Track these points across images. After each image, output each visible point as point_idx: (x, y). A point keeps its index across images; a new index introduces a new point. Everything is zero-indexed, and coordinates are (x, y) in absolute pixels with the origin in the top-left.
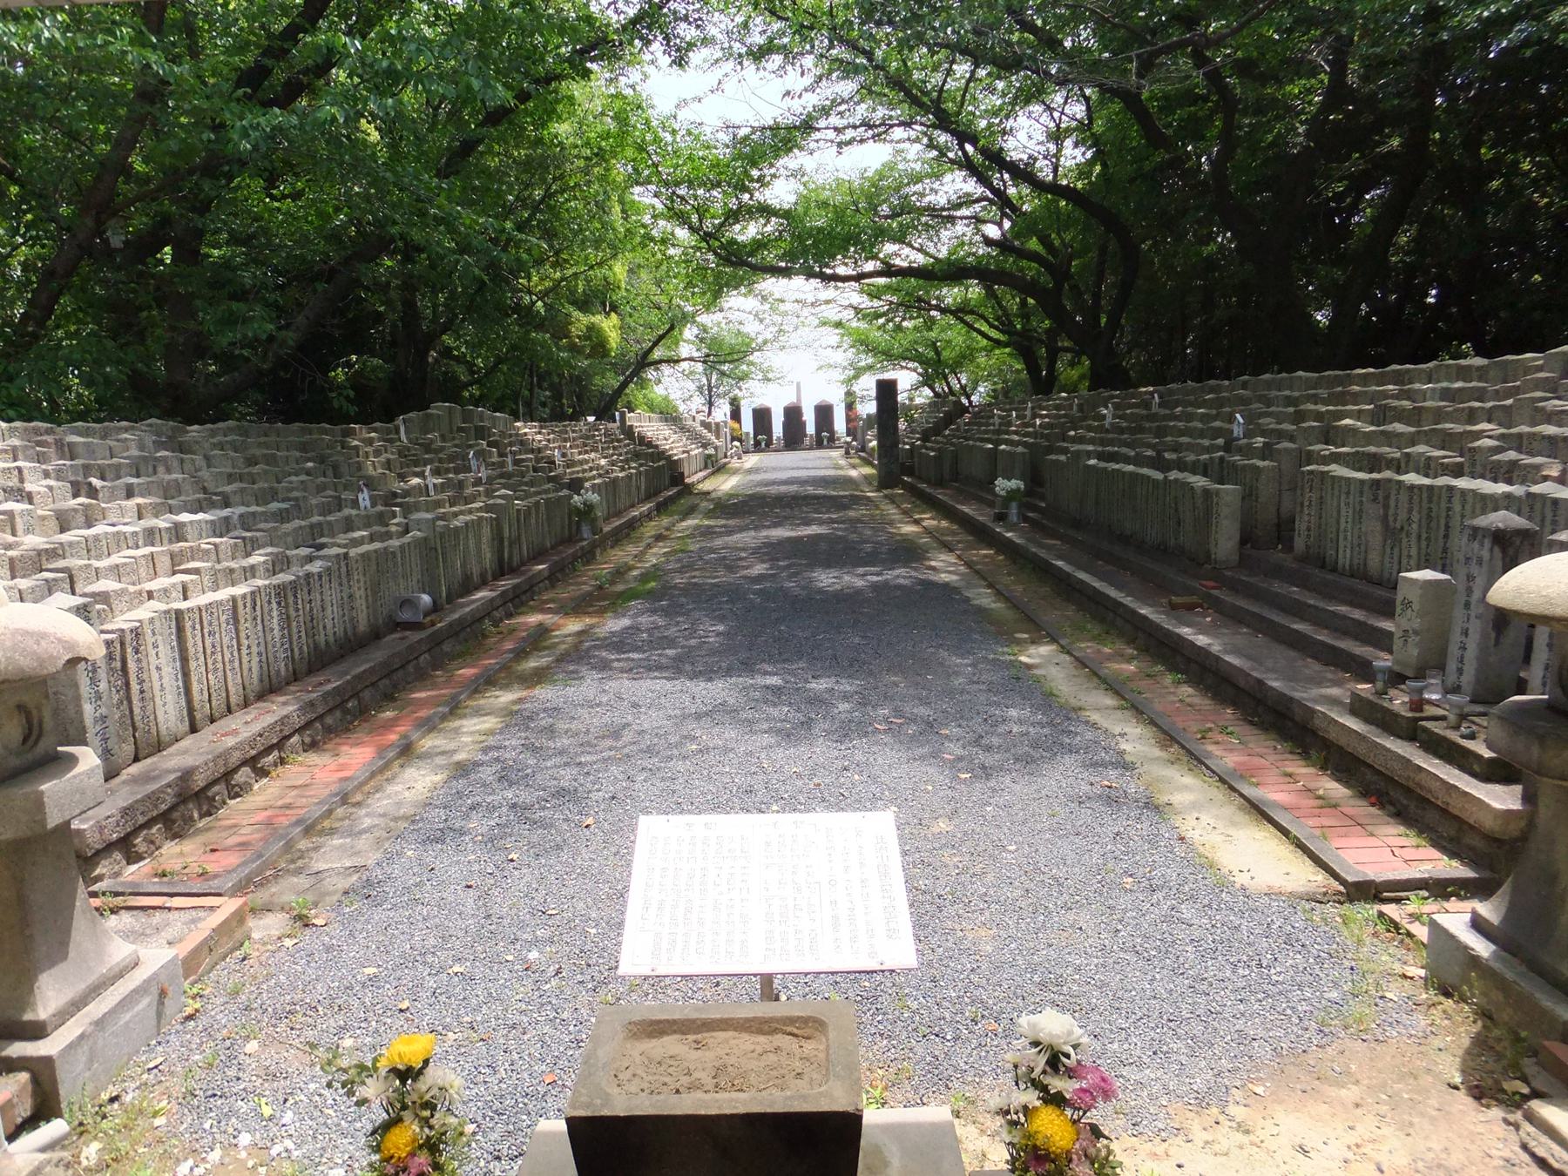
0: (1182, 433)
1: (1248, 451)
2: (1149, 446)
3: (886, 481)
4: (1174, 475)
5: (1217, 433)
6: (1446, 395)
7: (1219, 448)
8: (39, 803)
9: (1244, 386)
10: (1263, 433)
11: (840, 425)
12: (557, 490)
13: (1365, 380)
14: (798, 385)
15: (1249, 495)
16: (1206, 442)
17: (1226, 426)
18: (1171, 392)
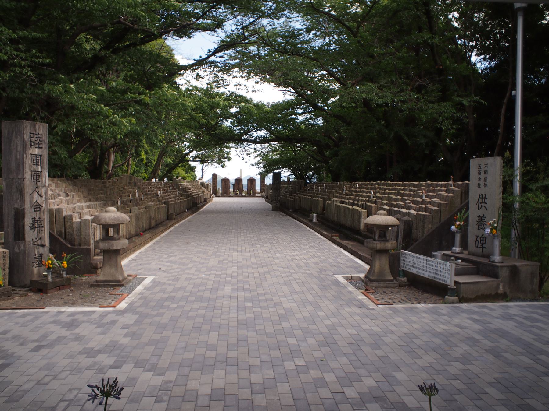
0: (361, 196)
1: (371, 202)
4: (354, 207)
6: (410, 191)
9: (378, 184)
11: (258, 188)
12: (159, 204)
13: (399, 185)
14: (241, 170)
16: (364, 199)
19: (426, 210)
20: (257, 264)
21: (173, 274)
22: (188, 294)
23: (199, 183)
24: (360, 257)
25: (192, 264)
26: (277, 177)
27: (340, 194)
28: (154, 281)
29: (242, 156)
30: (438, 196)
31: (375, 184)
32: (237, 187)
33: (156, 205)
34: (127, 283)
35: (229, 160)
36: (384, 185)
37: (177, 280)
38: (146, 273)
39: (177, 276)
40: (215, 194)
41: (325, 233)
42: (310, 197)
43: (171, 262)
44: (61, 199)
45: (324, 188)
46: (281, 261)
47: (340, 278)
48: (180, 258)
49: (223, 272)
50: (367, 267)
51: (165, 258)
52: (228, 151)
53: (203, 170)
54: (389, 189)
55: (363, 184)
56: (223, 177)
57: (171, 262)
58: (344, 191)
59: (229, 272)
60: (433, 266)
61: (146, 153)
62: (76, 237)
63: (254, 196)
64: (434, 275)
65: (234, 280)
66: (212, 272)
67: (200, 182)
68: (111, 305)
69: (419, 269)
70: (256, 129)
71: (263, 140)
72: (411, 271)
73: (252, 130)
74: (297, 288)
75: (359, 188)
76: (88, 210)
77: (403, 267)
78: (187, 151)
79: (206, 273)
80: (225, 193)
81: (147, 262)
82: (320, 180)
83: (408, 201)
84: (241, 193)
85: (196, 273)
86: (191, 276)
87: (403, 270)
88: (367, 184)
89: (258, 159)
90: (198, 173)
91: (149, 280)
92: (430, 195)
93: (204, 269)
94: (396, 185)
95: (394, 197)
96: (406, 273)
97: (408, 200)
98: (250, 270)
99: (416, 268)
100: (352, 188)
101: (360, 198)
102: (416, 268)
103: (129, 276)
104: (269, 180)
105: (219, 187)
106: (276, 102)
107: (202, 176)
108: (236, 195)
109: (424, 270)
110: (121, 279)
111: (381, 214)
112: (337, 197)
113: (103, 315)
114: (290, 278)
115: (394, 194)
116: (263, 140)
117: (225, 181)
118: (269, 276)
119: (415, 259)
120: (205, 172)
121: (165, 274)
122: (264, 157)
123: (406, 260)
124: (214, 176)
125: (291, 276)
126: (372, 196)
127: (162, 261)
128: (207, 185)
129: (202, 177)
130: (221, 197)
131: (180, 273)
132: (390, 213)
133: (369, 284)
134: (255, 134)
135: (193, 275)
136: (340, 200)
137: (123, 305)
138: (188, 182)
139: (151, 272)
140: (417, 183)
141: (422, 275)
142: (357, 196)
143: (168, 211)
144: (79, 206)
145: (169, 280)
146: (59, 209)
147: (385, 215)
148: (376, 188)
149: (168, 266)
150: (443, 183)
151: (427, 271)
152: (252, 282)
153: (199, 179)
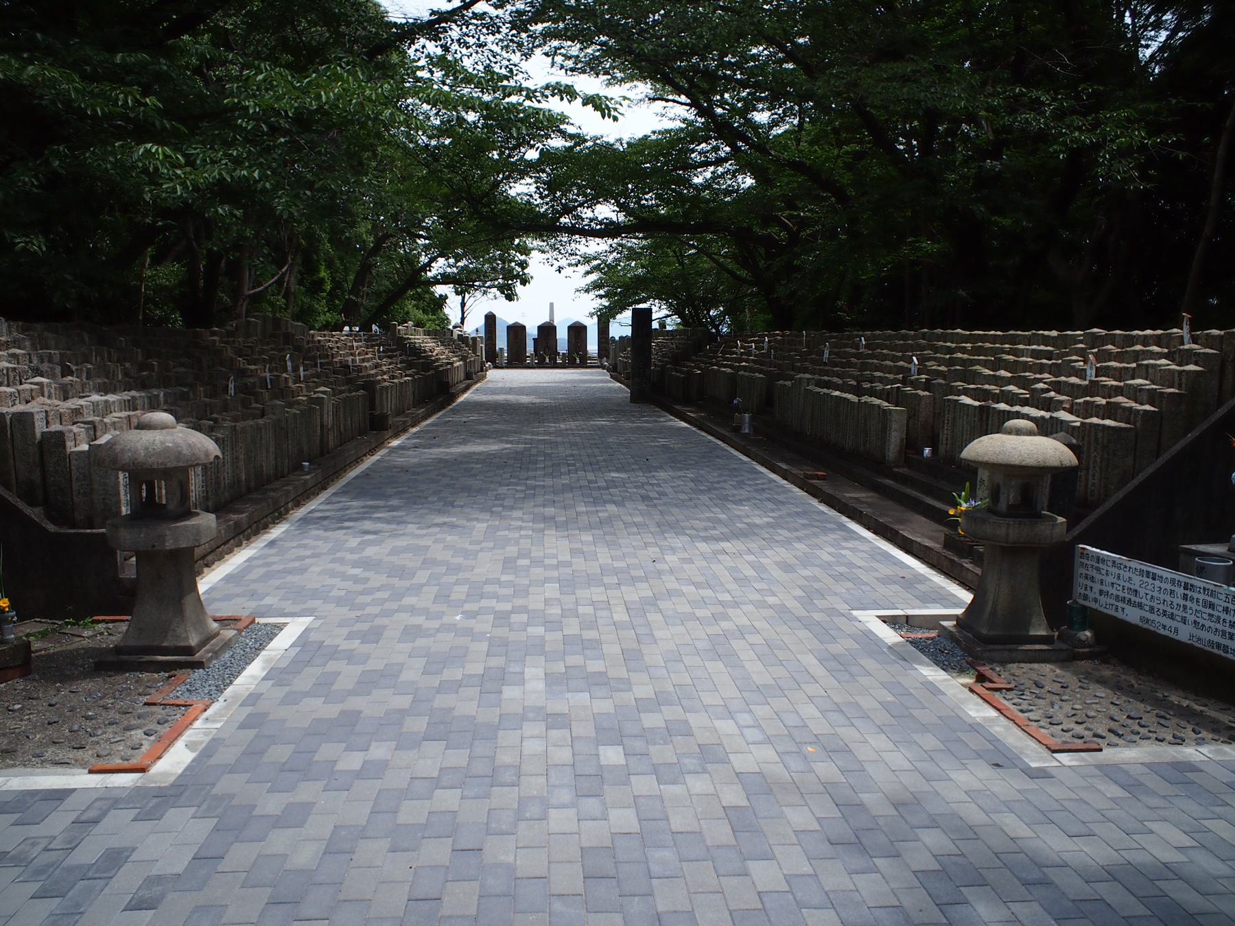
0: (877, 369)
1: (915, 384)
2: (853, 378)
3: (638, 397)
4: (865, 399)
5: (901, 370)
6: (1036, 354)
7: (898, 381)
8: (162, 537)
9: (924, 336)
10: (928, 372)
11: (592, 346)
12: (350, 392)
13: (994, 339)
14: (552, 305)
15: (912, 415)
16: (891, 376)
17: (906, 365)
18: (875, 337)
19: (1110, 411)
20: (616, 571)
21: (369, 610)
22: (404, 702)
23: (455, 337)
24: (907, 546)
25: (427, 573)
26: (641, 319)
27: (814, 362)
28: (302, 642)
29: (556, 264)
30: (1146, 372)
31: (914, 338)
32: (543, 347)
33: (341, 392)
34: (216, 654)
35: (524, 282)
36: (944, 338)
37: (374, 635)
38: (288, 606)
39: (379, 621)
40: (493, 362)
41: (784, 466)
42: (729, 370)
43: (367, 564)
44: (40, 384)
45: (766, 346)
46: (684, 560)
47: (870, 620)
48: (395, 552)
49: (519, 602)
50: (967, 597)
51: (352, 551)
52: (523, 257)
53: (463, 304)
54: (964, 351)
55: (875, 337)
56: (511, 322)
57: (367, 564)
58: (826, 355)
59: (535, 602)
60: (1212, 606)
61: (330, 265)
62: (76, 500)
63: (583, 365)
64: (1217, 639)
65: (553, 637)
66: (484, 603)
67: (456, 332)
68: (134, 762)
69: (1152, 609)
70: (592, 202)
71: (608, 230)
72: (1120, 615)
73: (581, 205)
74: (758, 672)
75: (866, 346)
76: (124, 414)
77: (1086, 597)
78: (424, 259)
79: (467, 607)
80: (517, 359)
81: (297, 564)
82: (739, 330)
83: (1041, 385)
84: (553, 360)
85: (436, 608)
86: (419, 620)
87: (1084, 608)
88: (889, 337)
89: (594, 277)
90: (452, 310)
91: (293, 629)
92: (1116, 369)
93: (460, 592)
94: (984, 339)
95: (987, 372)
96: (1091, 618)
97: (1040, 380)
98: (597, 594)
99: (1140, 606)
100: (846, 346)
101: (878, 374)
102: (1140, 606)
103: (224, 621)
104: (621, 326)
105: (502, 342)
106: (639, 135)
107: (463, 319)
108: (541, 365)
109: (1172, 617)
110: (193, 641)
111: (1019, 432)
112: (805, 371)
113: (91, 814)
114: (725, 625)
115: (985, 364)
116: (608, 230)
117: (517, 331)
118: (659, 617)
119: (1137, 579)
120: (470, 312)
121: (344, 611)
122: (608, 270)
123: (1098, 577)
124: (490, 319)
125: (726, 617)
126: (914, 369)
127: (342, 561)
128: (474, 339)
129: (462, 322)
130: (507, 367)
131: (388, 605)
132: (1046, 428)
133: (973, 647)
134: (587, 213)
135: (426, 612)
136: (816, 377)
137: (176, 760)
138: (428, 333)
139: (300, 601)
140: (1054, 333)
141: (1162, 632)
142: (864, 367)
143: (372, 406)
144: (95, 405)
145: (350, 636)
146: (22, 414)
147: (1030, 433)
148: (923, 348)
149: (356, 580)
150: (1149, 332)
151: (1184, 621)
152: (612, 649)
153: (455, 327)
